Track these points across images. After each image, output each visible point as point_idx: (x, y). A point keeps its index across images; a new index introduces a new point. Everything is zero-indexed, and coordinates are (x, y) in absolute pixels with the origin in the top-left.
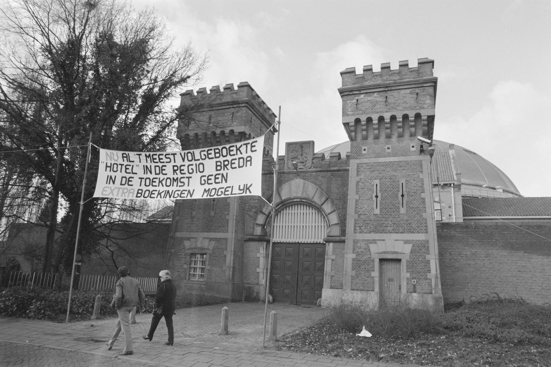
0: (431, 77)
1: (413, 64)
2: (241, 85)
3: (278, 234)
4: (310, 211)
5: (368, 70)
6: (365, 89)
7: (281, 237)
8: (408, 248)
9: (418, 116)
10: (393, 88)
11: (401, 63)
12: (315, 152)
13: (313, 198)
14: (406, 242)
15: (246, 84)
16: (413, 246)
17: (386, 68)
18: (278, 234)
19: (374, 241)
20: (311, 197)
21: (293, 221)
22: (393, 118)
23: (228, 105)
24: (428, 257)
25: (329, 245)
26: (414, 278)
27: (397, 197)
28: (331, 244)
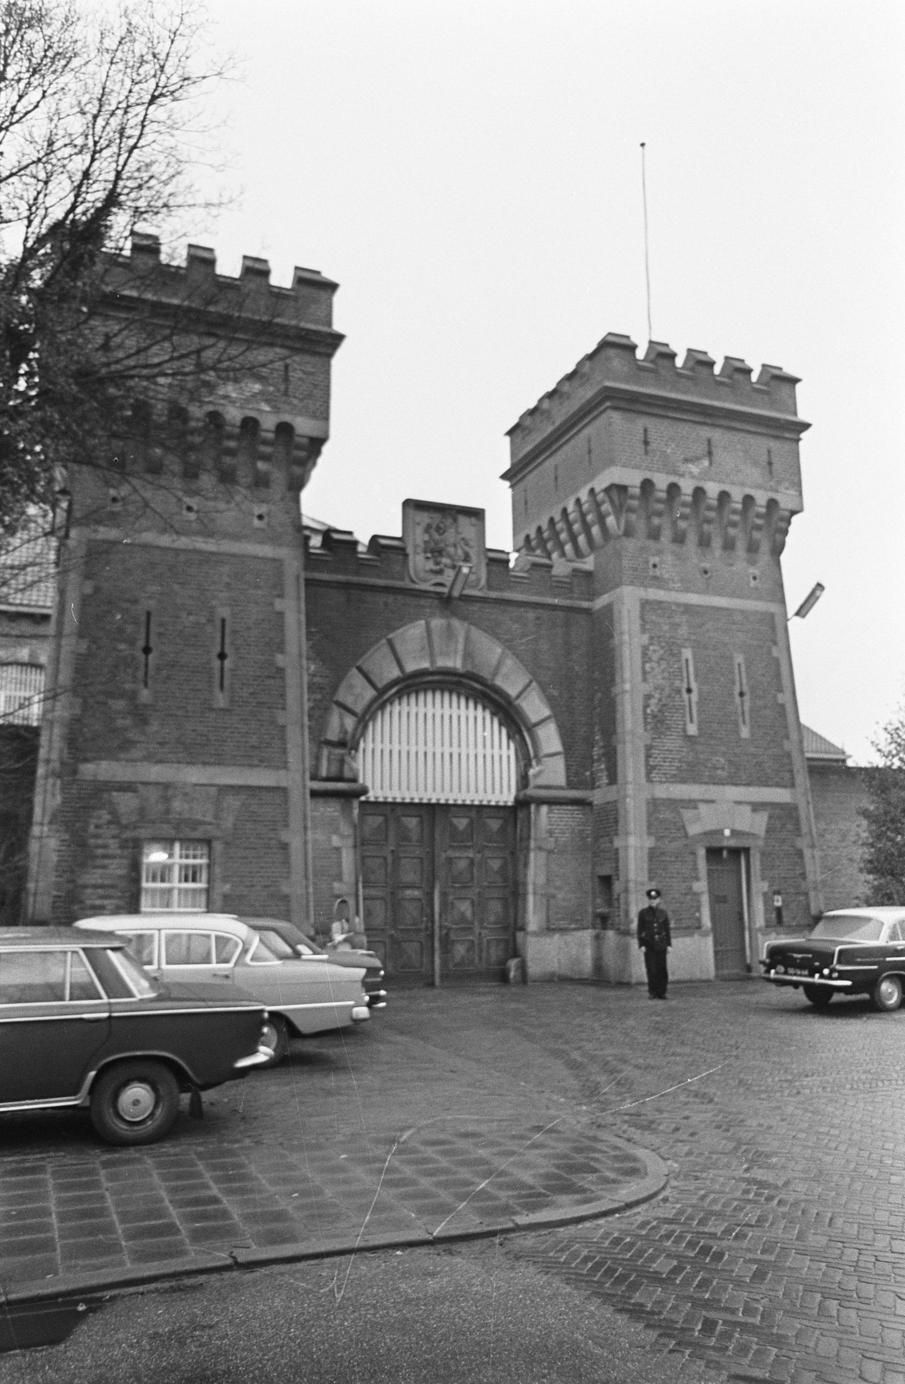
0: (324, 329)
1: (282, 278)
4: (430, 710)
8: (758, 824)
11: (250, 263)
12: (489, 545)
14: (757, 807)
15: (624, 341)
16: (770, 817)
19: (692, 804)
20: (485, 674)
21: (455, 741)
22: (673, 489)
23: (767, 426)
25: (537, 810)
26: (778, 893)
27: (731, 695)
28: (544, 809)
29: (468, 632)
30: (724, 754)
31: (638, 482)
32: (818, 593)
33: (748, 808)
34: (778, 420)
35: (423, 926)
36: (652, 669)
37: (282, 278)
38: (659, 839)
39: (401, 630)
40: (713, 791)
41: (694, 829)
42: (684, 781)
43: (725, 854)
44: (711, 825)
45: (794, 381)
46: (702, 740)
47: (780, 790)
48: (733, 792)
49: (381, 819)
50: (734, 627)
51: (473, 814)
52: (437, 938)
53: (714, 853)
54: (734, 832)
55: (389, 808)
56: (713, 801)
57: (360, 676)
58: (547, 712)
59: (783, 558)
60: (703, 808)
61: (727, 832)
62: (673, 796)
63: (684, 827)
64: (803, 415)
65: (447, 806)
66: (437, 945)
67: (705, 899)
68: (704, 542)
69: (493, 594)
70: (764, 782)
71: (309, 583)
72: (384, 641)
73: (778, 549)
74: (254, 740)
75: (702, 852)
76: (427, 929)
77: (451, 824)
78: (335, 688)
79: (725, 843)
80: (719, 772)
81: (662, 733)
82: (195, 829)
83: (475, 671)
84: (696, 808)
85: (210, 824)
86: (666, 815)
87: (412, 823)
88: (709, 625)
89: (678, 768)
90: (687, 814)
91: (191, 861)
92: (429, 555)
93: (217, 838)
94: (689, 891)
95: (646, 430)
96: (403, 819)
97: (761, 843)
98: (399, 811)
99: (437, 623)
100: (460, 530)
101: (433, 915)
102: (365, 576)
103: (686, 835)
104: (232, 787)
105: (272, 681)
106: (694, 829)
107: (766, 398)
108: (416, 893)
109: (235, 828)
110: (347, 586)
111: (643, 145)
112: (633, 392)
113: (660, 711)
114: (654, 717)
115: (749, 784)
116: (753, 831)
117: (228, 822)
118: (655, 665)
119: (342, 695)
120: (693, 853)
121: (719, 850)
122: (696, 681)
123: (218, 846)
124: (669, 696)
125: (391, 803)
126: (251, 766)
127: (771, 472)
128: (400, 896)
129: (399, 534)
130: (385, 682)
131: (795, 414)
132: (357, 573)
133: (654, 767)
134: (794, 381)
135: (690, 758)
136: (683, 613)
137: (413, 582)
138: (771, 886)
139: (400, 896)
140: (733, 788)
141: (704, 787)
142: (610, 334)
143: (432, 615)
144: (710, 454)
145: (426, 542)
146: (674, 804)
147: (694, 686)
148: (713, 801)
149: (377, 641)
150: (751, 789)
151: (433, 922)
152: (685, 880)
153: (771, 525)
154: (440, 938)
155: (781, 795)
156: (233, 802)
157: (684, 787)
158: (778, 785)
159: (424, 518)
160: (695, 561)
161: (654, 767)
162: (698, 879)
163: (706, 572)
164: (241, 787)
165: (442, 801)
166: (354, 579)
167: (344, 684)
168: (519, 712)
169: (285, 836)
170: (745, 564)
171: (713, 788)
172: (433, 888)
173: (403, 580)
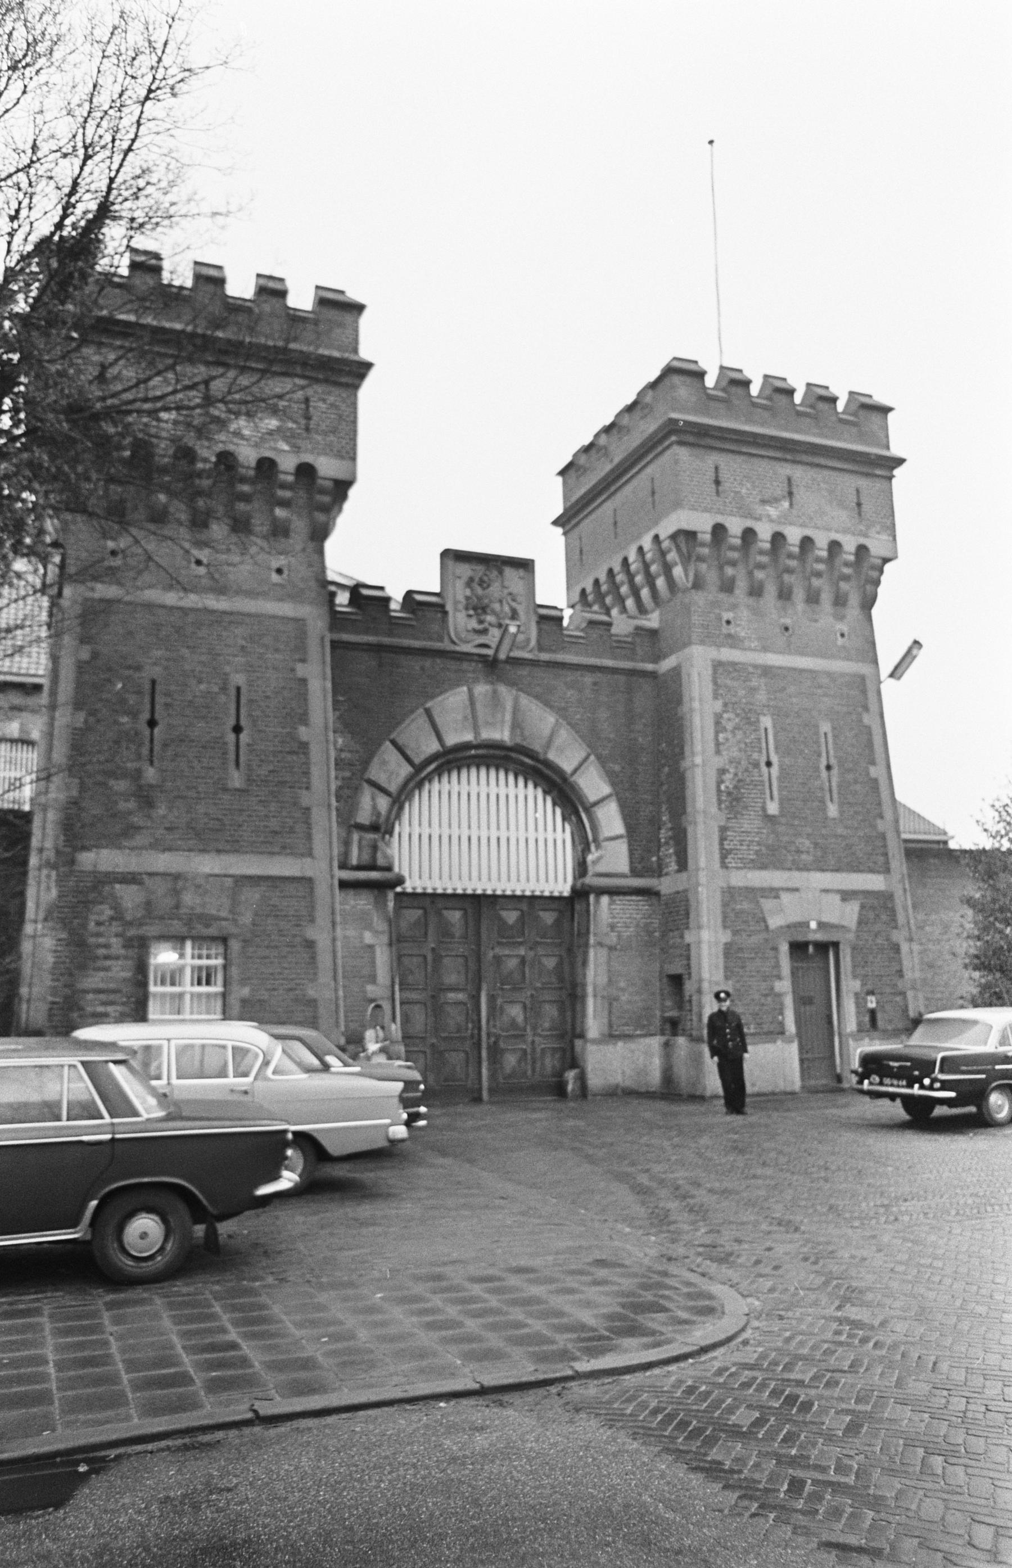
1: (301, 299)
8: (849, 915)
14: (846, 896)
16: (863, 907)
19: (774, 893)
25: (597, 901)
29: (516, 701)
32: (915, 652)
33: (838, 897)
36: (727, 740)
38: (735, 933)
40: (796, 878)
41: (775, 922)
42: (763, 867)
43: (811, 949)
47: (870, 876)
49: (420, 912)
52: (484, 1045)
53: (798, 948)
54: (821, 925)
56: (797, 890)
57: (395, 751)
58: (606, 789)
59: (875, 611)
60: (785, 897)
61: (813, 925)
62: (750, 884)
63: (764, 920)
66: (484, 1054)
67: (789, 1001)
68: (785, 595)
69: (545, 656)
70: (855, 868)
72: (421, 710)
74: (274, 824)
75: (784, 948)
76: (472, 1036)
77: (500, 918)
78: (366, 763)
80: (804, 857)
82: (207, 926)
83: (525, 744)
84: (777, 897)
87: (455, 916)
89: (757, 853)
90: (767, 904)
94: (771, 992)
96: (445, 912)
97: (851, 936)
99: (481, 689)
101: (479, 1021)
103: (767, 927)
105: (295, 758)
106: (775, 922)
108: (461, 996)
113: (736, 787)
114: (729, 794)
115: (837, 871)
117: (247, 919)
118: (730, 736)
120: (775, 949)
122: (777, 752)
123: (235, 945)
124: (746, 770)
125: (479, 896)
130: (423, 757)
132: (390, 634)
133: (729, 852)
142: (675, 359)
143: (476, 680)
144: (790, 494)
145: (467, 598)
148: (797, 890)
151: (480, 1029)
152: (765, 978)
153: (861, 575)
155: (874, 882)
156: (252, 896)
158: (871, 871)
159: (465, 570)
161: (729, 852)
162: (779, 977)
163: (787, 629)
165: (489, 892)
166: (386, 640)
169: (311, 933)
170: (831, 619)
171: (796, 874)
173: (441, 640)
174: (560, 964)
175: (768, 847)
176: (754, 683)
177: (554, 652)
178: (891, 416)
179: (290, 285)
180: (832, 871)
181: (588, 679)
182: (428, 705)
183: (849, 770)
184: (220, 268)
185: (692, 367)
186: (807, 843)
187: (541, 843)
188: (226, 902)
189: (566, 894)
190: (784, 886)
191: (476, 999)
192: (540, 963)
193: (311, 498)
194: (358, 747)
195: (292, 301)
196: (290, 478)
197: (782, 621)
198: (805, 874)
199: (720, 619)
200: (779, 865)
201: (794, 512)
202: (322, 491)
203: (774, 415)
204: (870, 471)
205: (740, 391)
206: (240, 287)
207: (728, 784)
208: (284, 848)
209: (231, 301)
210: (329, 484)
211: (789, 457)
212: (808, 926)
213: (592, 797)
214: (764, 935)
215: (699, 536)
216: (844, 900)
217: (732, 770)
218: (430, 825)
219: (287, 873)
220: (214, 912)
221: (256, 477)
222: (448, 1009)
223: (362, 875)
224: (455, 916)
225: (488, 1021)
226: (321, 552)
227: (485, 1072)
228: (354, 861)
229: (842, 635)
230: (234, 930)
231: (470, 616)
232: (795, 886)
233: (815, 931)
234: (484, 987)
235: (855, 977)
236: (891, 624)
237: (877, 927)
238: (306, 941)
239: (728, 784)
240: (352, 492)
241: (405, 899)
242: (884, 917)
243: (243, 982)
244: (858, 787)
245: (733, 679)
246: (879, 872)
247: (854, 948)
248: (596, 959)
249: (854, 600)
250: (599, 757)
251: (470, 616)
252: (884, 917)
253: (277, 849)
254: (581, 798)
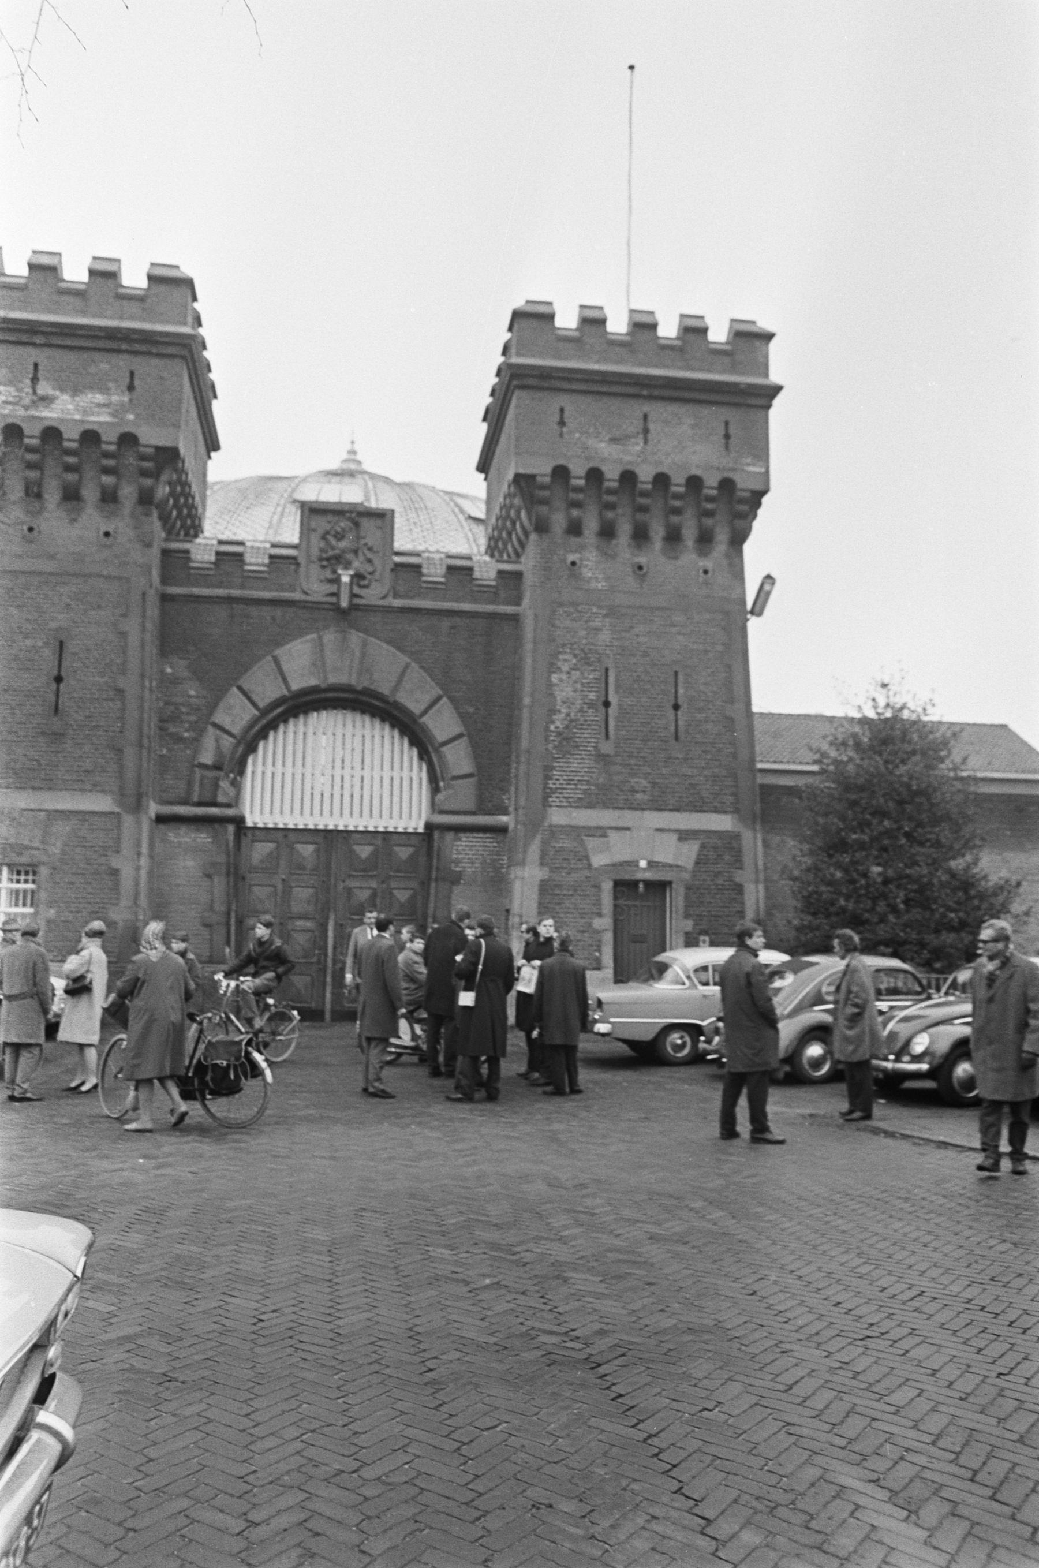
1: (134, 278)
2: (530, 309)
3: (258, 796)
4: (359, 732)
5: (593, 321)
6: (587, 381)
7: (277, 810)
8: (687, 855)
9: (561, 473)
10: (558, 384)
12: (398, 545)
13: (395, 689)
14: (684, 836)
16: (703, 846)
17: (104, 275)
18: (258, 796)
19: (601, 832)
20: (385, 689)
24: (739, 877)
25: (442, 838)
29: (365, 644)
30: (646, 776)
31: (547, 469)
32: (767, 587)
33: (675, 837)
34: (736, 385)
35: (314, 960)
36: (561, 680)
37: (134, 278)
38: (552, 870)
39: (287, 647)
40: (628, 817)
41: (599, 860)
42: (591, 806)
43: (641, 886)
44: (621, 854)
45: (769, 337)
46: (619, 759)
47: (714, 817)
48: (655, 819)
49: (272, 845)
50: (674, 630)
51: (320, 839)
52: (329, 971)
53: (625, 887)
54: (651, 864)
55: (280, 834)
56: (628, 829)
57: (241, 696)
58: (457, 728)
59: (748, 547)
60: (613, 835)
61: (643, 864)
62: (574, 823)
63: (587, 857)
64: (775, 377)
65: (347, 833)
66: (329, 979)
67: (608, 937)
68: (641, 536)
69: (398, 603)
70: (698, 806)
71: (165, 598)
72: (269, 658)
73: (739, 538)
74: (87, 764)
75: (607, 886)
76: (319, 962)
77: (352, 851)
78: (212, 708)
79: (640, 876)
80: (639, 796)
81: (568, 752)
82: (20, 854)
83: (372, 687)
84: (605, 836)
85: (37, 849)
86: (567, 843)
87: (307, 850)
88: (640, 629)
89: (585, 791)
90: (591, 843)
91: (22, 886)
92: (325, 563)
93: (44, 863)
94: (588, 928)
95: (562, 410)
96: (298, 846)
97: (687, 876)
98: (291, 835)
99: (330, 637)
100: (362, 534)
101: (326, 949)
102: (251, 588)
103: (590, 865)
104: (62, 812)
105: (111, 704)
106: (599, 860)
107: (727, 360)
108: (309, 924)
109: (63, 853)
110: (230, 600)
111: (631, 67)
112: (540, 367)
113: (567, 727)
114: (559, 734)
115: (677, 810)
116: (679, 863)
117: (56, 849)
118: (564, 677)
119: (220, 717)
120: (597, 887)
121: (635, 884)
122: (617, 692)
123: (44, 871)
124: (581, 710)
125: (331, 831)
126: (83, 790)
127: (727, 447)
128: (290, 927)
129: (296, 540)
130: (267, 701)
131: (767, 375)
132: (242, 587)
133: (553, 791)
134: (769, 337)
135: (601, 780)
136: (606, 616)
137: (306, 593)
138: (696, 925)
139: (290, 927)
140: (656, 814)
141: (617, 813)
142: (528, 302)
143: (326, 627)
144: (646, 431)
145: (322, 550)
146: (577, 832)
147: (613, 698)
148: (628, 829)
149: (260, 658)
150: (677, 815)
151: (326, 955)
152: (583, 915)
153: (730, 506)
154: (334, 972)
155: (722, 822)
156: (62, 828)
157: (590, 812)
158: (716, 811)
159: (322, 524)
160: (628, 556)
161: (553, 791)
162: (600, 915)
163: (640, 568)
164: (71, 812)
165: (341, 828)
166: (235, 592)
167: (222, 706)
168: (424, 729)
169: (115, 862)
170: (694, 556)
171: (628, 813)
172: (327, 918)
173: (294, 591)
174: (413, 897)
175: (597, 785)
176: (597, 623)
177: (411, 598)
178: (773, 345)
179: (709, 321)
180: (671, 810)
181: (446, 623)
182: (276, 653)
183: (700, 710)
184: (652, 313)
185: (173, 273)
186: (644, 782)
187: (396, 783)
188: (38, 833)
189: (421, 830)
190: (613, 824)
191: (323, 927)
192: (391, 893)
193: (666, 503)
194: (205, 693)
195: (559, 322)
196: (682, 490)
197: (636, 560)
198: (638, 813)
199: (564, 561)
200: (609, 804)
201: (649, 448)
202: (741, 501)
203: (633, 352)
204: (742, 401)
205: (646, 335)
206: (75, 272)
207: (558, 724)
208: (94, 785)
209: (560, 332)
210: (747, 495)
211: (645, 393)
212: (637, 866)
213: (440, 736)
214: (586, 873)
215: (539, 479)
216: (680, 839)
217: (564, 710)
218: (274, 765)
219: (97, 809)
220: (26, 842)
221: (552, 482)
222: (295, 935)
223: (200, 811)
224: (307, 850)
225: (335, 948)
226: (740, 553)
227: (328, 995)
228: (195, 799)
229: (706, 572)
230: (44, 858)
231: (323, 567)
232: (625, 825)
233: (644, 870)
234: (332, 916)
235: (687, 916)
236: (759, 555)
237: (719, 867)
238: (110, 868)
239: (558, 724)
240: (765, 500)
241: (257, 833)
242: (727, 857)
243: (50, 905)
244: (709, 726)
245: (574, 620)
246: (725, 812)
247: (688, 888)
248: (437, 892)
249: (722, 536)
250: (452, 699)
251: (323, 567)
252: (727, 857)
253: (88, 786)
254: (431, 738)
